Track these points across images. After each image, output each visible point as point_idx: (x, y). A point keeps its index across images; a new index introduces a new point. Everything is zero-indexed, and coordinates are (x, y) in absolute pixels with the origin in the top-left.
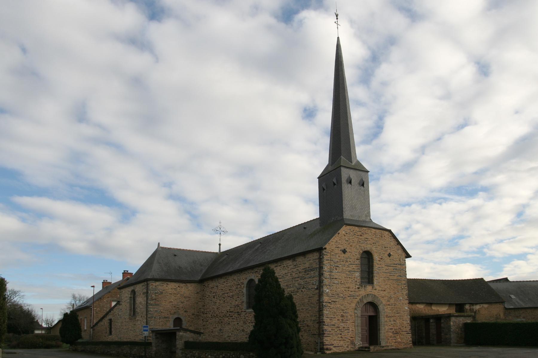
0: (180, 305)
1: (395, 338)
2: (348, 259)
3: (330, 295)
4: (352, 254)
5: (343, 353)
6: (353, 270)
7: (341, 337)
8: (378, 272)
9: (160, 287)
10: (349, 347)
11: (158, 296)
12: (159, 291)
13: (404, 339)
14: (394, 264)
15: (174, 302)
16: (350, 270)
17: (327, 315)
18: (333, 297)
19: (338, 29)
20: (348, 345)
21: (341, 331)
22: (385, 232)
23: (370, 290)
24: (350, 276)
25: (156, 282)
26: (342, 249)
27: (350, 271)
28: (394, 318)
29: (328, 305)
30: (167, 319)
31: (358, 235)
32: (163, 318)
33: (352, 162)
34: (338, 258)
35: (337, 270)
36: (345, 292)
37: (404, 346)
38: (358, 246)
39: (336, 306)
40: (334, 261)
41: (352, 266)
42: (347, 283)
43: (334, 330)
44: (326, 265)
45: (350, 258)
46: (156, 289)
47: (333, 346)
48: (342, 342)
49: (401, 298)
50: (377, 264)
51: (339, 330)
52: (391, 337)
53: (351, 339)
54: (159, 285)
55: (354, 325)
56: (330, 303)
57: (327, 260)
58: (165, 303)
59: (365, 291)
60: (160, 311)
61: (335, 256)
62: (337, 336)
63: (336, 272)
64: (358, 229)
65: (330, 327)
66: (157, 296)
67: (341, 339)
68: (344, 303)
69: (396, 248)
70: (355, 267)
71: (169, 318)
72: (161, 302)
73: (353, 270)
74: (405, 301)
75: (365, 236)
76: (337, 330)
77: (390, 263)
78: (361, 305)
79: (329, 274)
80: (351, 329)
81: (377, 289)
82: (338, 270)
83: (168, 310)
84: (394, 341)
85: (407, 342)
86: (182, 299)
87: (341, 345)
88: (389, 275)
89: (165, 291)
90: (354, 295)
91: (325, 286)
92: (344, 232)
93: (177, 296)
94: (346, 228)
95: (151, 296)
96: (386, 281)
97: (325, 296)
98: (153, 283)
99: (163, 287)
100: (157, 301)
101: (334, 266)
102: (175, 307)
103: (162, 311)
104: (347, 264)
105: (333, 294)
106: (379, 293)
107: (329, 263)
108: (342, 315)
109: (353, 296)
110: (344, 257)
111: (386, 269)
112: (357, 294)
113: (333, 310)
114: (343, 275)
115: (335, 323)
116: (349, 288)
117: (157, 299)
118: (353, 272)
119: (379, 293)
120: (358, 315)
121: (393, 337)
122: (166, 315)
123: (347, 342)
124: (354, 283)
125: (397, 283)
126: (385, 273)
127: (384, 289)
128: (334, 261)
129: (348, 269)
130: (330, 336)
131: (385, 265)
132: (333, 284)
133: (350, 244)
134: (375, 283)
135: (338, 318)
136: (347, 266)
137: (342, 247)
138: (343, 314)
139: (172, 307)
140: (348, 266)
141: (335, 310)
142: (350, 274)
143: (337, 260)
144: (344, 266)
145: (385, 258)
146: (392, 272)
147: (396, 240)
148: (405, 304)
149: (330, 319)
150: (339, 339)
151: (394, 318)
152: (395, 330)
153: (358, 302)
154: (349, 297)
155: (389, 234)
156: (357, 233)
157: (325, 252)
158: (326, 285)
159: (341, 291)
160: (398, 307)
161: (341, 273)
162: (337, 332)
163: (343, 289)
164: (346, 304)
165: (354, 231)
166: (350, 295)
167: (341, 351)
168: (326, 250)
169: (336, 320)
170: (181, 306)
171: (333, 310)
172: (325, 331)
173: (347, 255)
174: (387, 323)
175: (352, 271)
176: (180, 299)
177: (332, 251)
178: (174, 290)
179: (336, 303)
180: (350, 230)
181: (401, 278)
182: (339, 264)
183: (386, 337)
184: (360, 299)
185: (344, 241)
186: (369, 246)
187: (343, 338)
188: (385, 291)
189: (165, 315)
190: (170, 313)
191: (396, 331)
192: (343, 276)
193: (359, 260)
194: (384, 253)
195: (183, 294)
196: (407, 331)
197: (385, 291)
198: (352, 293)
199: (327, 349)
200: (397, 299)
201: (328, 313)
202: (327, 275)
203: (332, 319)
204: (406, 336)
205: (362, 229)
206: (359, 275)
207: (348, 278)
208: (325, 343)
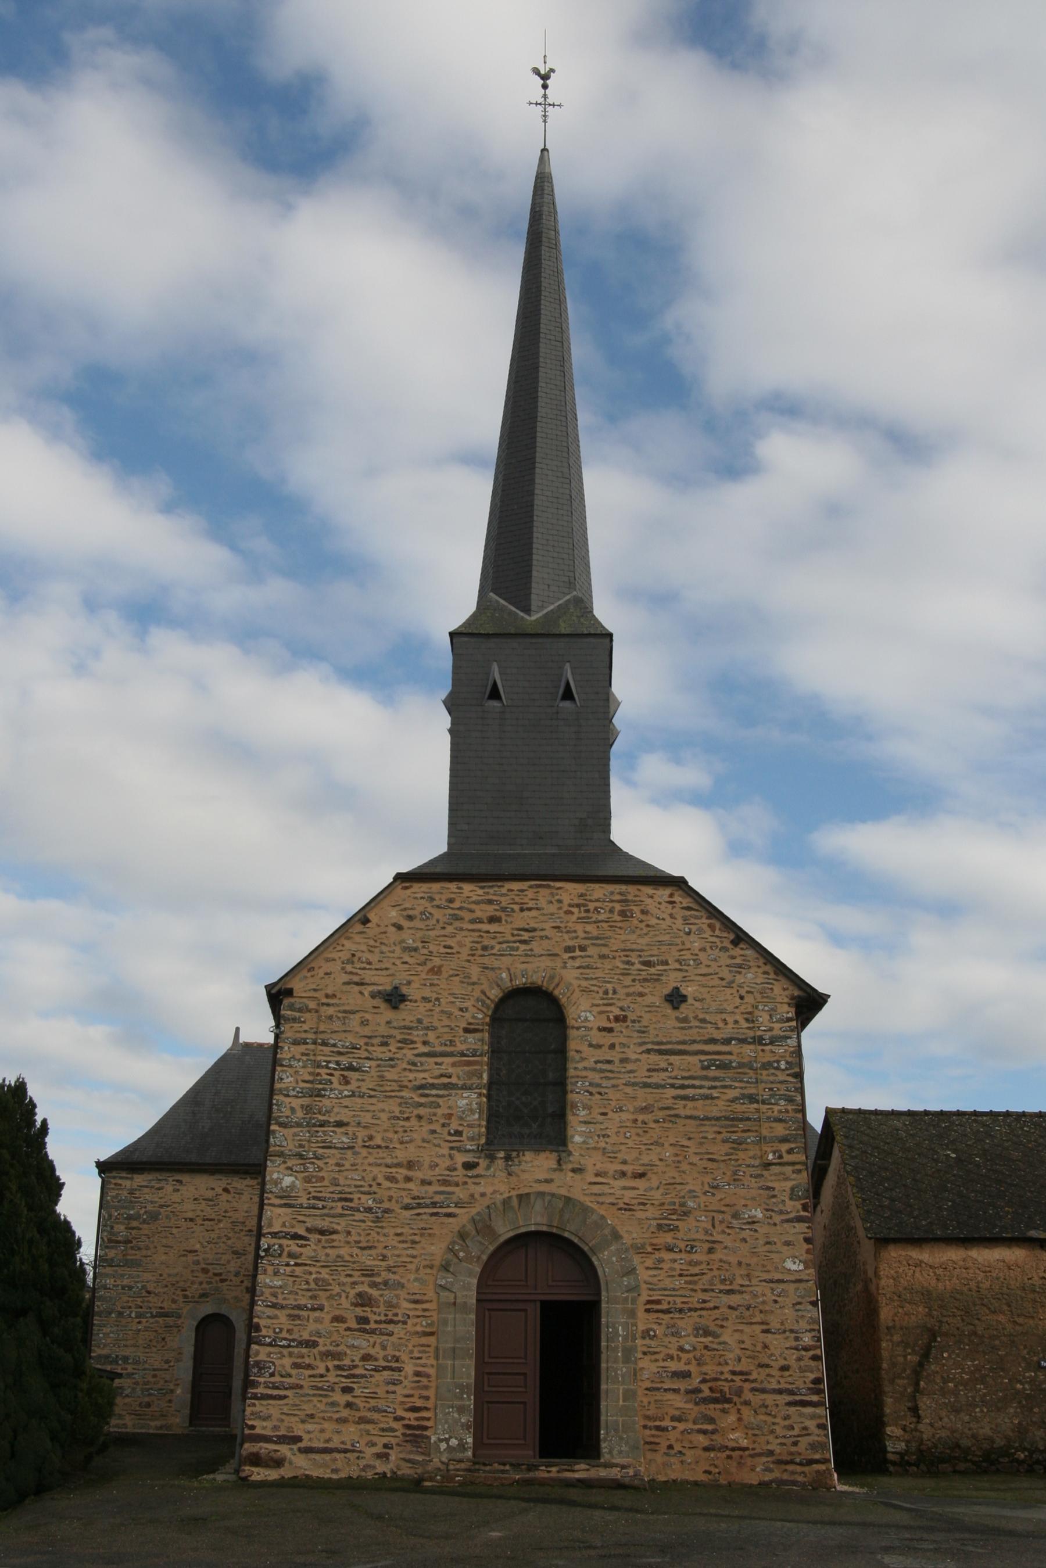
0: (229, 1262)
1: (710, 1427)
2: (415, 1033)
3: (304, 1201)
4: (437, 1009)
5: (351, 1485)
6: (445, 1080)
7: (349, 1405)
8: (599, 1085)
9: (147, 1195)
10: (393, 1458)
11: (141, 1229)
12: (142, 1211)
13: (772, 1432)
14: (713, 1041)
15: (205, 1253)
16: (424, 1082)
17: (275, 1295)
18: (318, 1212)
19: (545, 121)
20: (385, 1446)
21: (354, 1376)
22: (648, 890)
23: (542, 1176)
24: (422, 1111)
25: (135, 1176)
26: (380, 988)
27: (422, 1087)
28: (700, 1316)
29: (287, 1249)
30: (170, 1321)
31: (473, 921)
32: (153, 1316)
33: (527, 610)
34: (358, 1029)
35: (347, 1083)
36: (387, 1184)
37: (771, 1471)
38: (475, 971)
39: (328, 1251)
40: (334, 1045)
41: (436, 1064)
42: (402, 1143)
43: (309, 1367)
44: (290, 1066)
45: (427, 1028)
46: (131, 1202)
47: (295, 1447)
48: (350, 1433)
49: (759, 1214)
50: (591, 1045)
51: (338, 1368)
52: (678, 1419)
53: (412, 1415)
54: (147, 1187)
55: (431, 1350)
56: (296, 1237)
57: (296, 1043)
58: (164, 1257)
59: (513, 1179)
60: (144, 1287)
61: (344, 1024)
62: (325, 1400)
63: (346, 1093)
64: (481, 892)
65: (285, 1351)
66: (133, 1228)
67: (345, 1413)
68: (382, 1239)
69: (725, 960)
70: (454, 1065)
71: (179, 1317)
72: (149, 1253)
73: (445, 1080)
74: (785, 1225)
75: (521, 920)
76: (328, 1370)
77: (678, 1035)
78: (482, 1249)
79: (302, 1106)
80: (409, 1369)
81: (591, 1170)
82: (353, 1085)
83: (177, 1282)
84: (702, 1440)
85: (792, 1454)
86: (239, 1238)
87: (343, 1443)
88: (674, 1098)
89: (169, 1209)
90: (438, 1198)
91: (279, 1160)
92: (394, 913)
93: (216, 1227)
94: (408, 892)
95: (112, 1228)
96: (653, 1125)
97: (273, 1205)
98: (119, 1181)
99: (161, 1193)
100: (132, 1248)
101: (331, 1065)
102: (205, 1271)
103: (151, 1287)
104: (409, 1054)
105: (315, 1198)
106: (596, 1189)
107: (307, 1055)
108: (360, 1295)
109: (434, 1204)
110: (395, 1024)
111: (649, 1070)
112: (460, 1193)
113: (313, 1269)
114: (381, 1106)
115: (319, 1334)
116: (410, 1165)
117: (134, 1242)
118: (441, 1092)
119: (596, 1189)
120: (455, 1298)
121: (694, 1423)
122: (165, 1305)
123: (383, 1430)
124: (443, 1144)
125: (725, 1135)
126: (646, 1085)
127: (641, 1170)
128: (334, 1045)
129: (411, 1076)
130: (285, 1397)
131: (644, 1048)
132: (323, 1147)
133: (429, 965)
134: (578, 1139)
135: (337, 1313)
136: (405, 1066)
137: (382, 980)
138: (371, 1291)
139: (192, 1271)
140: (414, 1064)
141: (324, 1271)
142: (423, 1100)
143: (350, 1039)
144: (392, 1067)
145: (647, 1017)
146: (697, 1083)
147: (723, 923)
148: (787, 1243)
149: (290, 1316)
150: (336, 1416)
151: (700, 1316)
152: (704, 1381)
153: (462, 1235)
154: (407, 1207)
155: (677, 898)
156: (472, 911)
157: (291, 1007)
158: (281, 1154)
159: (363, 1179)
160: (733, 1260)
161: (370, 1097)
162: (322, 1376)
163: (376, 1170)
164: (393, 1241)
165: (457, 904)
166: (414, 1198)
167: (343, 1475)
168: (292, 1000)
169: (328, 1318)
170: (232, 1267)
171: (311, 1273)
172: (255, 1370)
173: (406, 1015)
174: (653, 1343)
175: (433, 1086)
176: (229, 1239)
177: (325, 1000)
178: (204, 1202)
179: (334, 1237)
180: (432, 899)
181: (758, 1110)
182: (366, 1054)
183: (648, 1418)
184: (473, 1219)
185: (398, 949)
186: (546, 963)
187: (358, 1410)
188: (642, 1175)
189: (162, 1302)
190: (186, 1297)
191: (711, 1389)
192: (383, 1111)
193: (478, 1035)
194: (641, 989)
195: (241, 1220)
196: (791, 1392)
197: (642, 1175)
198: (427, 1188)
199: (256, 1460)
200: (728, 1217)
201: (281, 1287)
202: (293, 1110)
203: (301, 1313)
204: (787, 1418)
205: (504, 890)
206: (479, 1104)
207: (408, 1119)
208: (253, 1427)
